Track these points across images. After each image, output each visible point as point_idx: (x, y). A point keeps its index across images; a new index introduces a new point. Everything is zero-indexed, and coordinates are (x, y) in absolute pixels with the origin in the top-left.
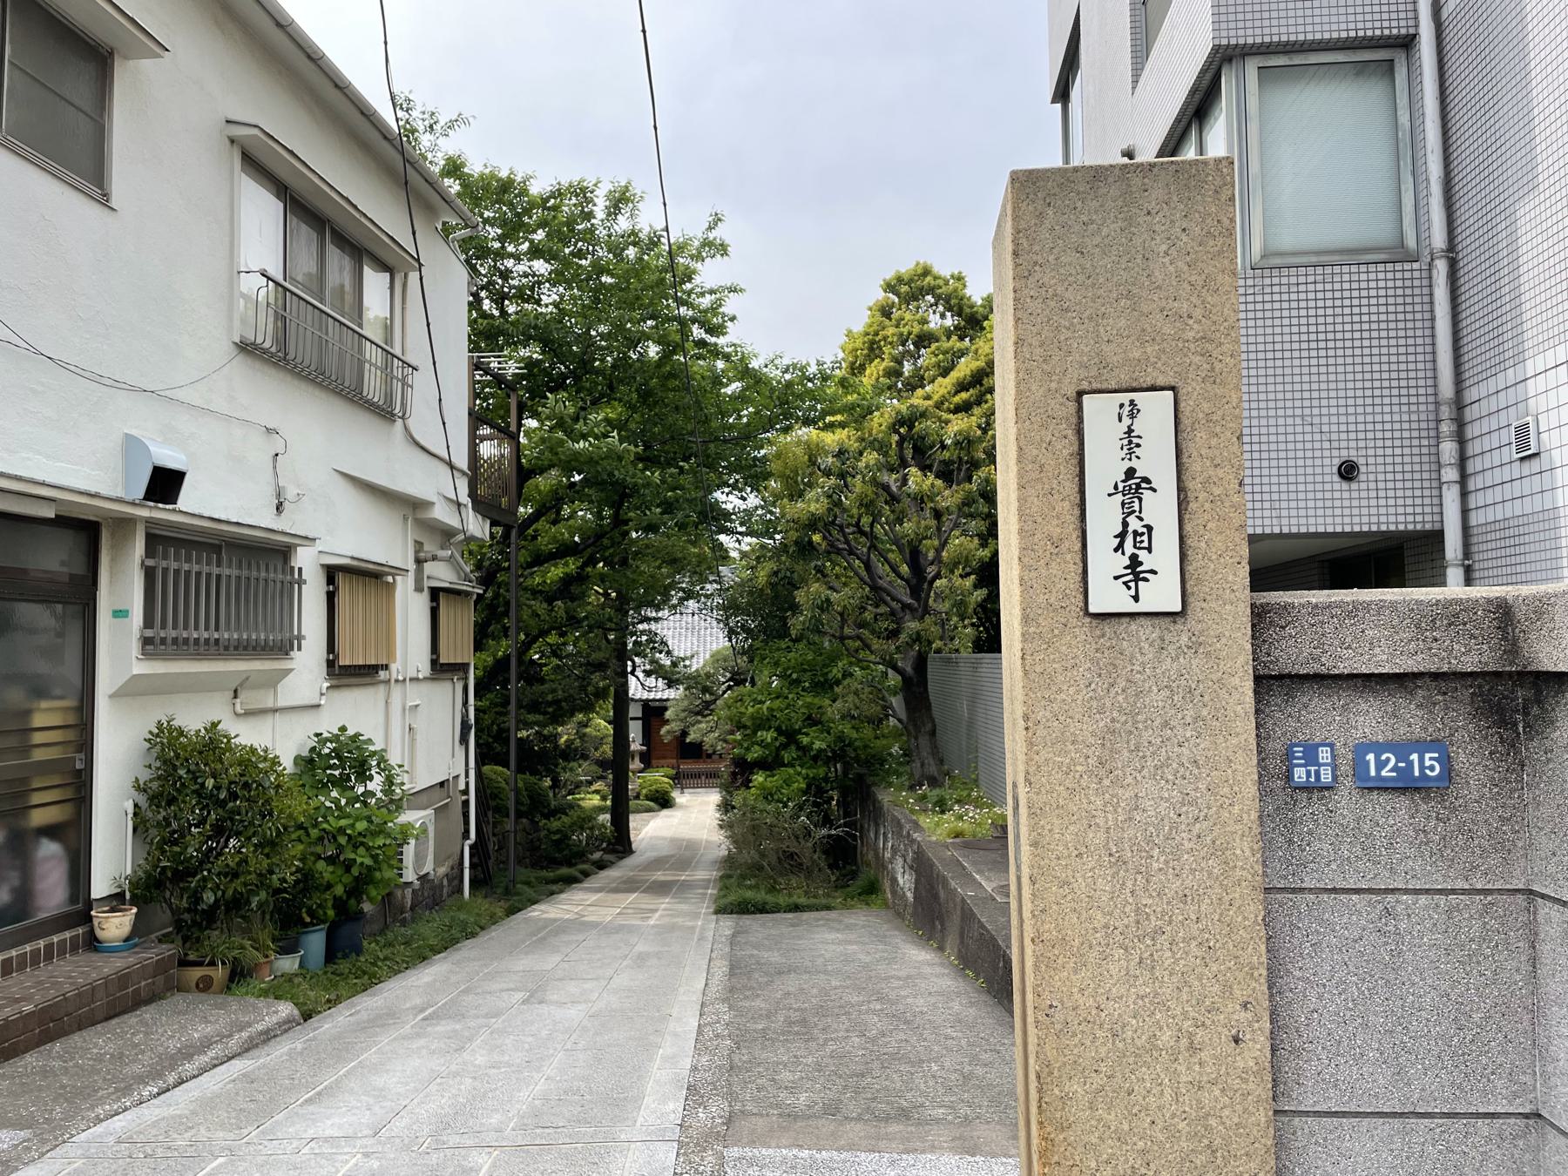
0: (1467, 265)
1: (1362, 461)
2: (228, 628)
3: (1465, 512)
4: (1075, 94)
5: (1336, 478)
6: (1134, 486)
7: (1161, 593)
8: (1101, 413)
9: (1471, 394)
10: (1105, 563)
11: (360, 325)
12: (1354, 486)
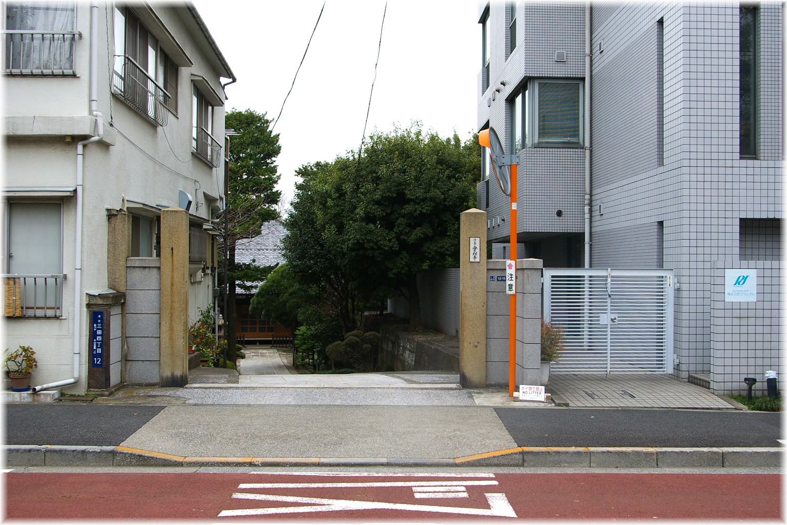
0: (595, 153)
1: (563, 210)
2: (611, 288)
3: (591, 227)
4: (488, 22)
5: (556, 215)
6: (475, 248)
7: (478, 260)
8: (472, 239)
9: (594, 192)
10: (472, 256)
11: (147, 72)
12: (561, 218)
